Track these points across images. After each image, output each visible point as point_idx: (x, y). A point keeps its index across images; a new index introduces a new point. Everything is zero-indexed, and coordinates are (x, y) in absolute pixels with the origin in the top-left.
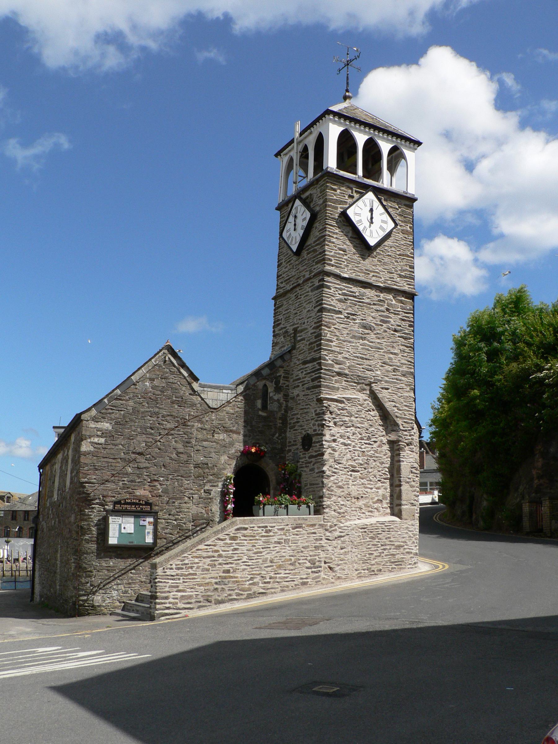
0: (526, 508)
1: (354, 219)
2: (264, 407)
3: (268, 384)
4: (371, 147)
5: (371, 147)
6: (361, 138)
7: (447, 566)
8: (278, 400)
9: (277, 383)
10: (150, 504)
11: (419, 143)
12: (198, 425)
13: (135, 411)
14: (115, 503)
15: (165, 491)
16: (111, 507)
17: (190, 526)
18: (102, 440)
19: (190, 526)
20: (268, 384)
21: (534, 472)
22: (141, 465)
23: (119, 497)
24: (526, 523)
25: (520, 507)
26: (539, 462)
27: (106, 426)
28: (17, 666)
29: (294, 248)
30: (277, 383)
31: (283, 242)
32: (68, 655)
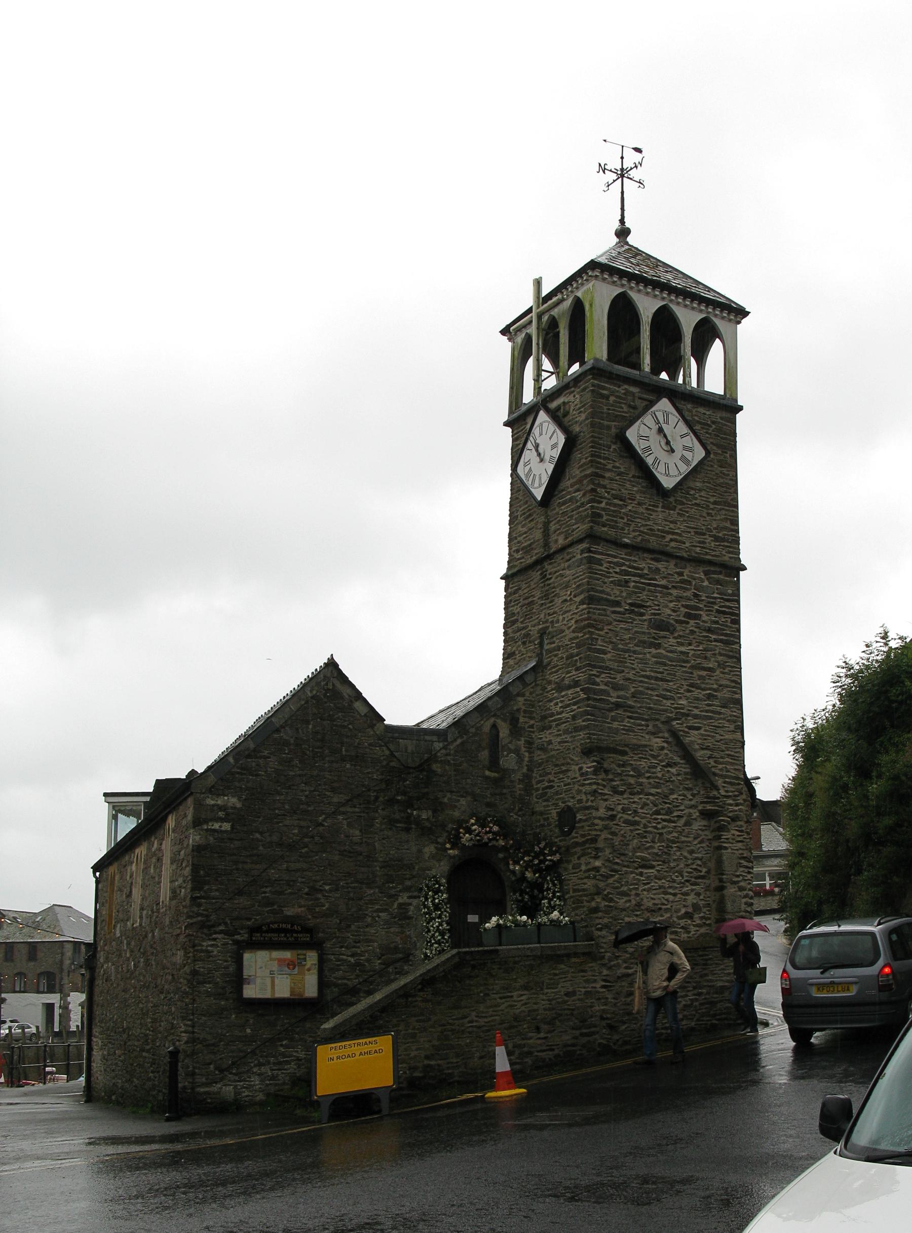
6: (647, 306)
14: (253, 930)
18: (227, 826)
27: (233, 801)
31: (518, 488)
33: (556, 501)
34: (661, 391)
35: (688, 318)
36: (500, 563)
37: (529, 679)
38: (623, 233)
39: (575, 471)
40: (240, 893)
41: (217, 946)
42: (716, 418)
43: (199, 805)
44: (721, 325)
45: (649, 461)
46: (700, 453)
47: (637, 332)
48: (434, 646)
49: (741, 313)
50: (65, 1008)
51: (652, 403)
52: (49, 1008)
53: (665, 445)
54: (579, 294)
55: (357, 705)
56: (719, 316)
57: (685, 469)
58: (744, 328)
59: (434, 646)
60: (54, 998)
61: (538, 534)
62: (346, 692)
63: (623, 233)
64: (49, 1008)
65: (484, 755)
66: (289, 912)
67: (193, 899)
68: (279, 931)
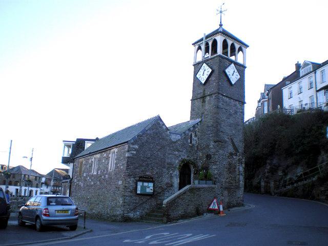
0: (263, 184)
1: (228, 73)
2: (191, 142)
3: (192, 133)
4: (233, 45)
5: (233, 45)
6: (230, 42)
7: (254, 206)
8: (196, 140)
9: (195, 133)
10: (152, 178)
11: (248, 46)
12: (168, 148)
13: (147, 142)
14: (140, 177)
15: (157, 173)
16: (138, 179)
17: (165, 187)
18: (135, 152)
19: (165, 187)
20: (192, 133)
21: (266, 170)
22: (149, 163)
23: (140, 175)
24: (263, 190)
25: (259, 183)
26: (268, 167)
27: (137, 147)
28: (172, 243)
29: (203, 82)
30: (195, 133)
31: (196, 79)
32: (179, 241)
33: (207, 84)
34: (232, 62)
35: (237, 46)
36: (190, 96)
37: (199, 124)
38: (221, 25)
39: (213, 78)
40: (137, 168)
41: (131, 181)
42: (241, 68)
43: (129, 147)
44: (243, 48)
45: (230, 77)
46: (239, 77)
47: (227, 48)
48: (177, 112)
49: (248, 46)
50: (21, 190)
51: (230, 64)
52: (17, 190)
53: (232, 72)
54: (216, 38)
55: (164, 127)
56: (243, 46)
57: (236, 80)
58: (247, 50)
59: (177, 112)
60: (18, 188)
61: (202, 91)
62: (161, 123)
63: (221, 25)
64: (17, 190)
65: (189, 141)
66: (147, 174)
67: (127, 169)
68: (146, 178)
